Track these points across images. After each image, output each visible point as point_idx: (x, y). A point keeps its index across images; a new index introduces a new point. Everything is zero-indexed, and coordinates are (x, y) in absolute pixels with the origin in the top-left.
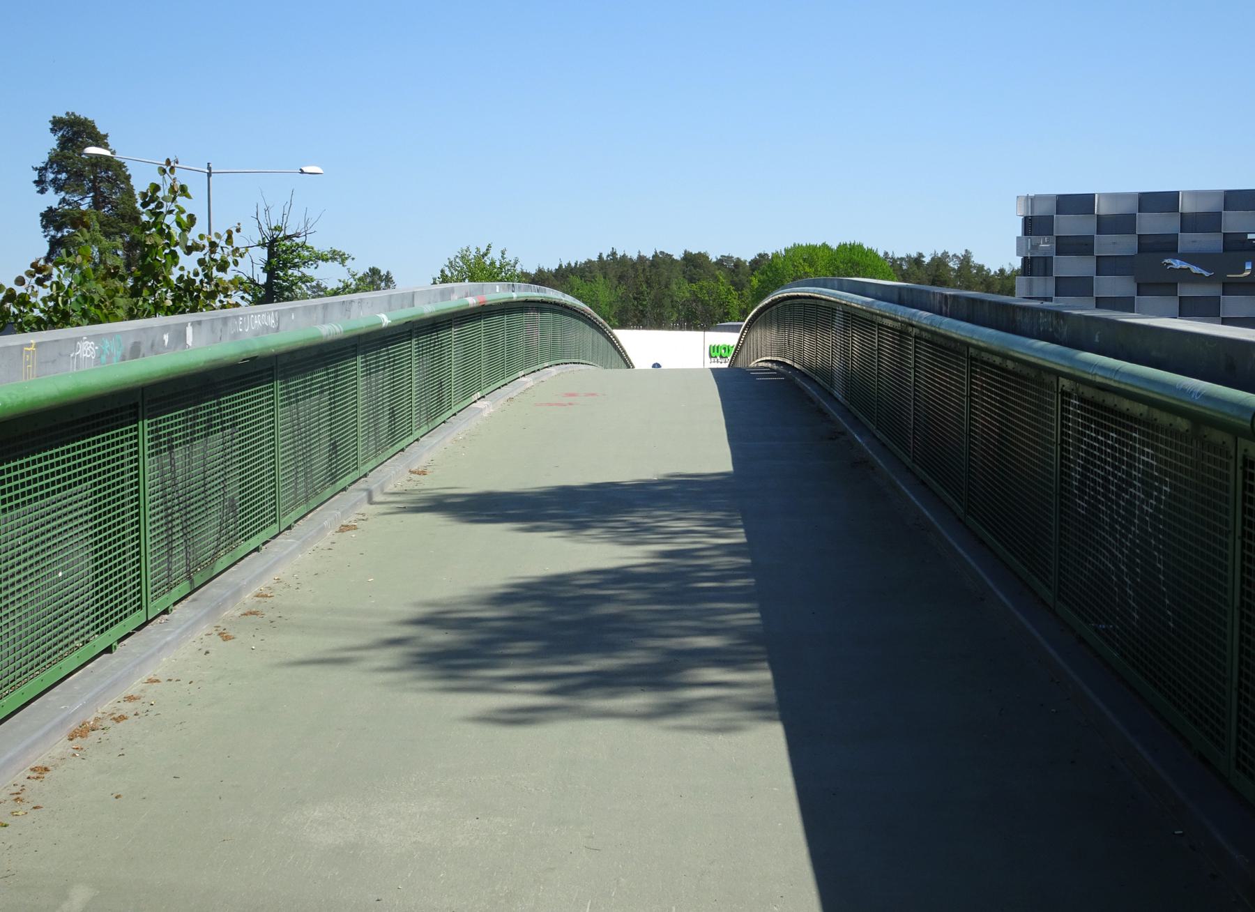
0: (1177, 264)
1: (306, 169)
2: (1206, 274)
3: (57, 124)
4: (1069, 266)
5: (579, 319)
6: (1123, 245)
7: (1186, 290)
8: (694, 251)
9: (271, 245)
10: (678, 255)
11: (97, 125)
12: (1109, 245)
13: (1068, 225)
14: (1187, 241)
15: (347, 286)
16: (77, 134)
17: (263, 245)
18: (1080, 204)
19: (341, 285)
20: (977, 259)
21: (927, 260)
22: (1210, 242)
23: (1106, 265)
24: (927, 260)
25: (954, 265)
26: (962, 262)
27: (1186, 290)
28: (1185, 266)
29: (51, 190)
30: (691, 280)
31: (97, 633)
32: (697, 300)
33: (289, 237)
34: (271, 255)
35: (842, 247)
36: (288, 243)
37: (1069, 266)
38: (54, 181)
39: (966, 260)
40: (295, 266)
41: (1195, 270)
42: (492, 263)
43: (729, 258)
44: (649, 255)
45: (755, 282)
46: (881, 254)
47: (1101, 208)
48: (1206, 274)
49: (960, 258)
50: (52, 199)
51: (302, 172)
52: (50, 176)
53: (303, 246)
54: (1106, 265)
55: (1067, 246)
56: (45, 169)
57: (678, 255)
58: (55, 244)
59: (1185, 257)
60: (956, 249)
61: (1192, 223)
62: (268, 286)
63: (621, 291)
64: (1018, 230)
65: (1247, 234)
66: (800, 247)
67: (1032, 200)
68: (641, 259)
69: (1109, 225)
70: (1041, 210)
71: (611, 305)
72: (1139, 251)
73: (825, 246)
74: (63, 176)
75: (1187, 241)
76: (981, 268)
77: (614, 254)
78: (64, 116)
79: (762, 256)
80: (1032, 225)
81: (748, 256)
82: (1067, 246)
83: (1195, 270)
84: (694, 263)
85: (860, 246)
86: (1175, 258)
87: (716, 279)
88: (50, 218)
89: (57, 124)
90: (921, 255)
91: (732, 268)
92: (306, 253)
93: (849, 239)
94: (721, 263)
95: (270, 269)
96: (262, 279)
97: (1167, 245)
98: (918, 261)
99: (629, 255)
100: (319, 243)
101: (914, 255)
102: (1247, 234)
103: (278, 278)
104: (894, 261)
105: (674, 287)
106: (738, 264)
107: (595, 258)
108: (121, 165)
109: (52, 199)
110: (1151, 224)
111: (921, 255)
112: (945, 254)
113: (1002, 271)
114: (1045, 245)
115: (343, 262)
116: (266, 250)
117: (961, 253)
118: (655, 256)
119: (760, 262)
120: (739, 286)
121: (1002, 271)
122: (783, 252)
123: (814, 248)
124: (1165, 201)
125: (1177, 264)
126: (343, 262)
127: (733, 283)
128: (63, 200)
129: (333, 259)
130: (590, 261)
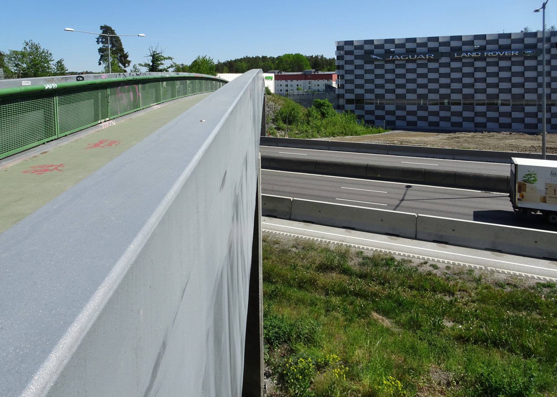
0: (374, 57)
1: (139, 35)
2: (381, 59)
3: (102, 28)
4: (348, 58)
5: (195, 79)
6: (361, 52)
7: (376, 63)
8: (264, 56)
9: (153, 56)
10: (261, 57)
11: (112, 27)
12: (357, 52)
13: (347, 48)
14: (376, 51)
15: (172, 65)
16: (107, 30)
17: (151, 56)
18: (350, 43)
19: (171, 65)
20: (324, 56)
21: (314, 56)
22: (381, 51)
23: (357, 57)
24: (314, 56)
25: (319, 57)
26: (321, 57)
27: (376, 63)
28: (376, 57)
29: (101, 43)
30: (263, 62)
31: (251, 90)
32: (265, 66)
33: (158, 54)
34: (153, 58)
35: (296, 54)
36: (157, 55)
37: (348, 58)
38: (102, 41)
39: (322, 57)
40: (159, 61)
41: (378, 58)
42: (207, 59)
43: (272, 57)
44: (255, 57)
45: (277, 62)
46: (304, 56)
47: (355, 44)
48: (381, 59)
49: (149, 65)
50: (101, 45)
51: (139, 36)
52: (100, 40)
53: (161, 56)
54: (357, 57)
55: (347, 53)
56: (99, 38)
57: (261, 57)
58: (102, 56)
59: (375, 55)
60: (320, 54)
61: (377, 47)
62: (153, 65)
63: (248, 64)
64: (336, 49)
65: (390, 49)
66: (287, 54)
67: (339, 42)
68: (253, 57)
69: (357, 48)
70: (341, 45)
71: (246, 67)
72: (451, 51)
73: (292, 54)
74: (104, 40)
75: (376, 51)
76: (325, 58)
77: (247, 56)
78: (103, 26)
79: (279, 56)
80: (339, 48)
81: (276, 56)
82: (347, 53)
83: (378, 58)
84: (264, 58)
85: (299, 54)
86: (373, 55)
87: (269, 61)
88: (100, 50)
89: (102, 28)
90: (312, 56)
91: (272, 59)
92: (162, 58)
93: (297, 53)
94: (270, 58)
95: (153, 61)
96: (151, 64)
97: (372, 52)
98: (312, 57)
99: (250, 57)
100: (165, 55)
101: (311, 56)
102: (390, 49)
103: (155, 64)
104: (307, 57)
105: (260, 63)
106: (274, 58)
107: (243, 57)
108: (118, 37)
109: (101, 45)
110: (367, 47)
111: (312, 56)
112: (318, 55)
113: (330, 59)
114: (342, 53)
115: (171, 59)
116: (152, 57)
117: (321, 55)
118: (256, 57)
119: (279, 58)
120: (274, 63)
121: (330, 59)
122: (41, 50)
123: (290, 54)
124: (371, 42)
125: (374, 57)
126: (171, 59)
127: (272, 62)
128: (104, 46)
129: (169, 59)
130: (242, 58)
